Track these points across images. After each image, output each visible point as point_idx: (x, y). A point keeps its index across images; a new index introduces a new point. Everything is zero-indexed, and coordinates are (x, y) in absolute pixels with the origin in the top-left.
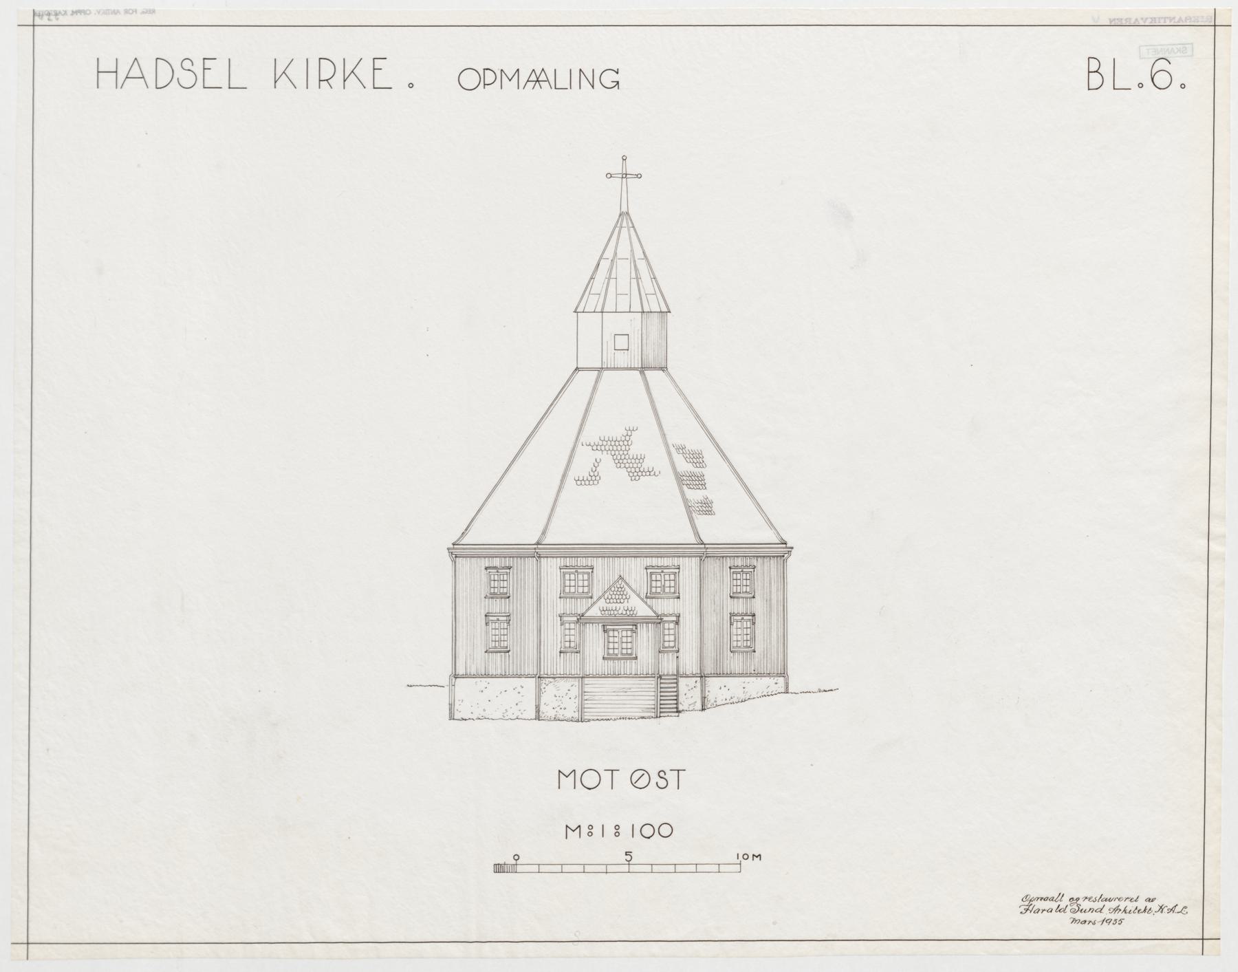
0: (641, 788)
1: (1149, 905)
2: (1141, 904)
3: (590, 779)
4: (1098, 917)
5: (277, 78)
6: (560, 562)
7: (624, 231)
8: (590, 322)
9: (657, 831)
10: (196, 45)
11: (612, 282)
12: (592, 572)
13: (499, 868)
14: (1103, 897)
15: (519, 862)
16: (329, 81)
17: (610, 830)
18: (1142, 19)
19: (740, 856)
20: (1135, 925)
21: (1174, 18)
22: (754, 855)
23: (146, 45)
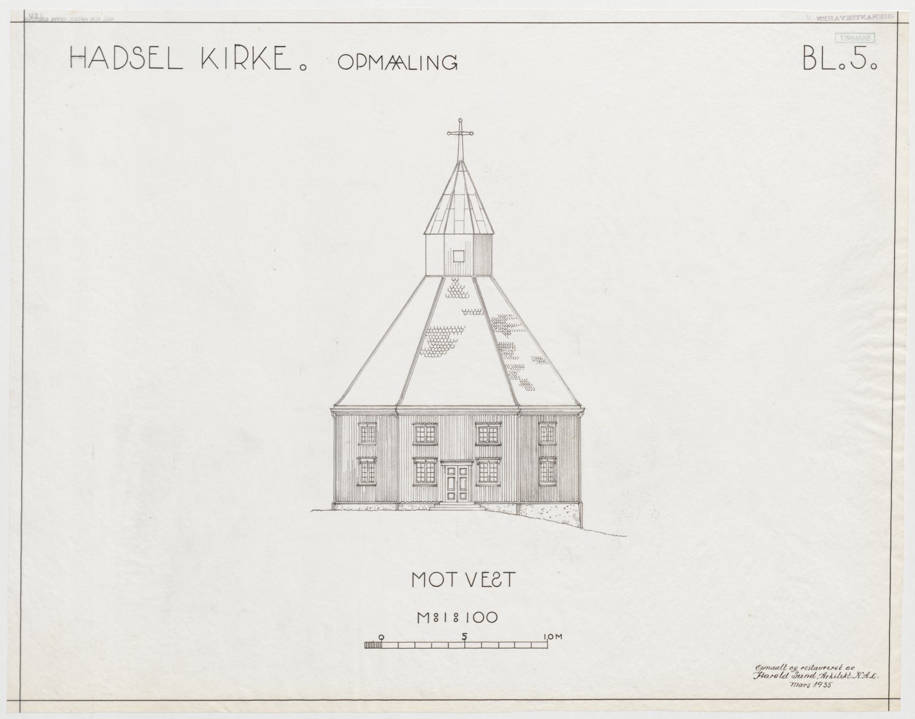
0: (433, 586)
1: (848, 672)
2: (844, 672)
3: (436, 580)
4: (812, 681)
5: (436, 65)
6: (413, 419)
7: (461, 174)
8: (435, 242)
9: (485, 617)
10: (143, 37)
11: (452, 211)
12: (376, 426)
13: (369, 645)
14: (814, 667)
15: (466, 641)
16: (243, 64)
17: (451, 617)
18: (841, 17)
19: (547, 637)
20: (839, 687)
21: (864, 16)
22: (556, 635)
23: (105, 37)
